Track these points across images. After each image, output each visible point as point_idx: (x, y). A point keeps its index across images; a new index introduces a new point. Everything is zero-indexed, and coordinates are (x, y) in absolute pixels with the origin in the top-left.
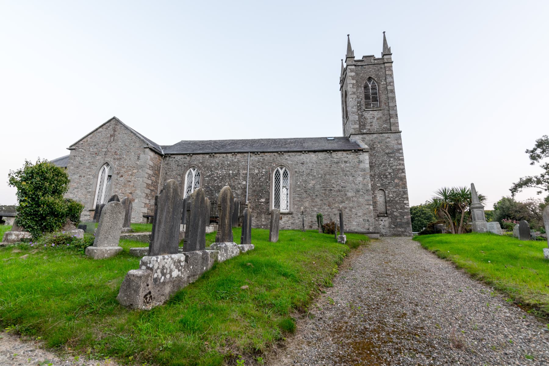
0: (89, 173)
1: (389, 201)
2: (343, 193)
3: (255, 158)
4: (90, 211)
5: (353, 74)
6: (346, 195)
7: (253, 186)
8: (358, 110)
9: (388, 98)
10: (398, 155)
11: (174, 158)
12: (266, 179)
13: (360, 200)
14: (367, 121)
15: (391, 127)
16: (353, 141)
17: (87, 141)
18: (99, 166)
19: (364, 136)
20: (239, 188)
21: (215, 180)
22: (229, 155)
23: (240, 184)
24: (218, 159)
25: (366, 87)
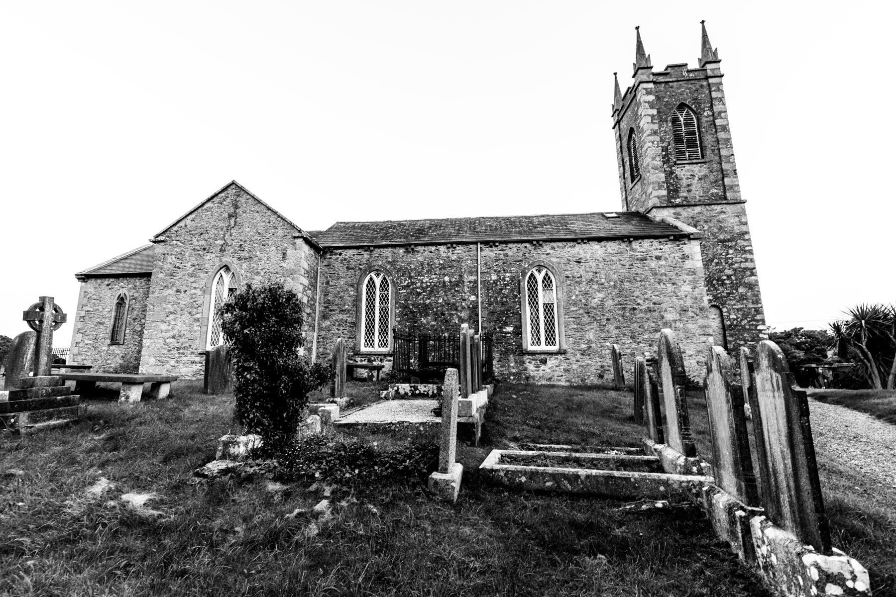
0: (194, 285)
1: (730, 326)
2: (656, 314)
3: (489, 253)
4: (200, 354)
5: (651, 98)
6: (663, 317)
7: (490, 304)
8: (664, 163)
9: (718, 141)
10: (741, 243)
11: (340, 254)
12: (512, 291)
13: (690, 326)
14: (681, 182)
15: (723, 193)
16: (658, 219)
17: (186, 226)
18: (211, 272)
19: (678, 210)
20: (463, 308)
21: (419, 294)
22: (442, 249)
23: (464, 300)
24: (422, 255)
25: (675, 121)
